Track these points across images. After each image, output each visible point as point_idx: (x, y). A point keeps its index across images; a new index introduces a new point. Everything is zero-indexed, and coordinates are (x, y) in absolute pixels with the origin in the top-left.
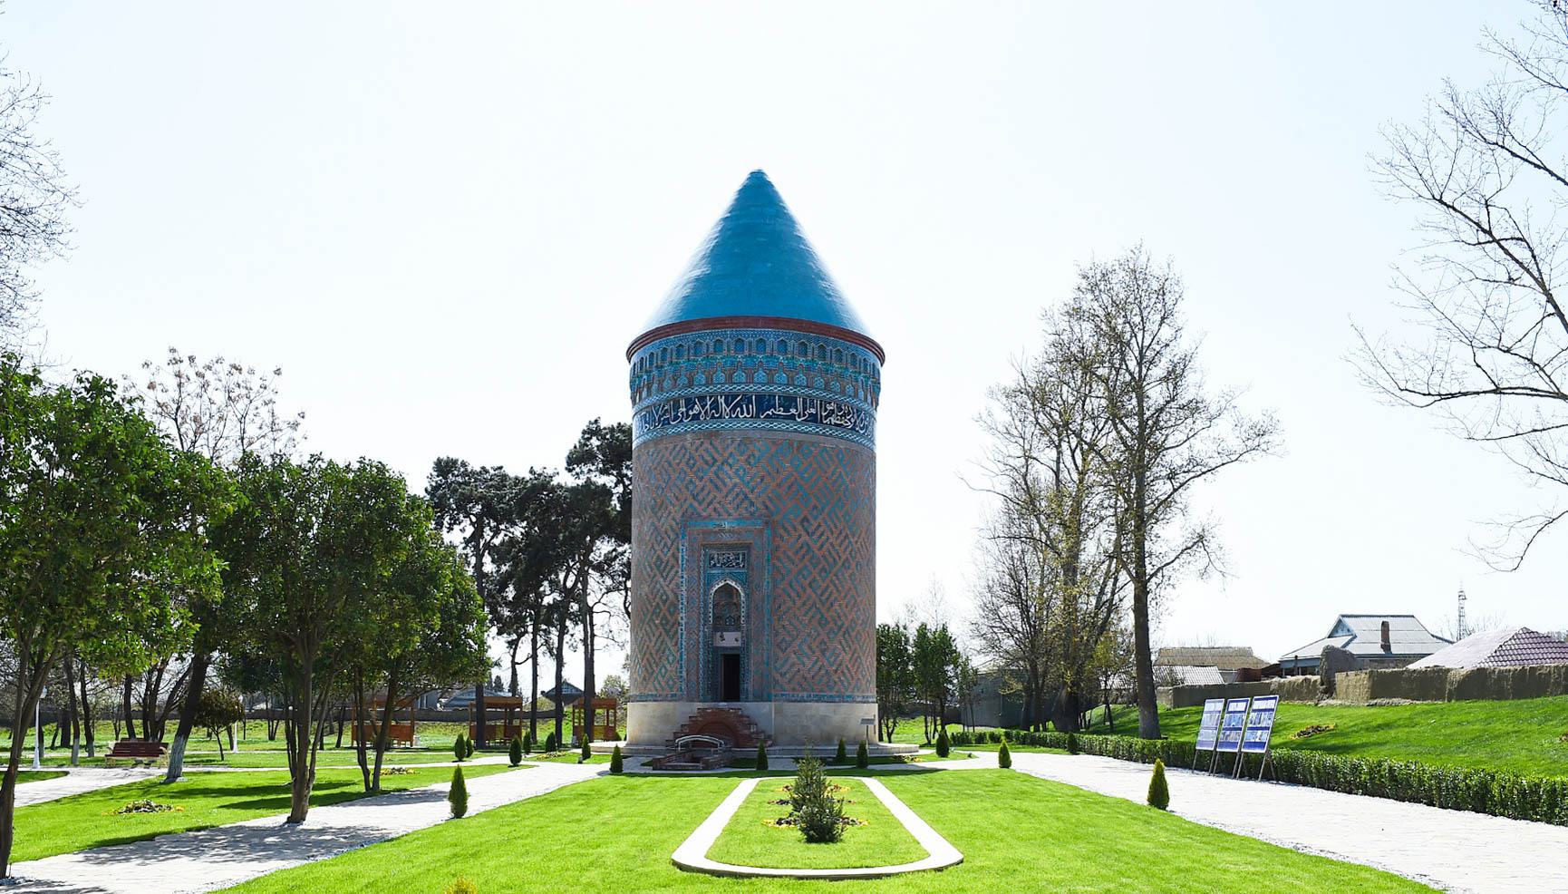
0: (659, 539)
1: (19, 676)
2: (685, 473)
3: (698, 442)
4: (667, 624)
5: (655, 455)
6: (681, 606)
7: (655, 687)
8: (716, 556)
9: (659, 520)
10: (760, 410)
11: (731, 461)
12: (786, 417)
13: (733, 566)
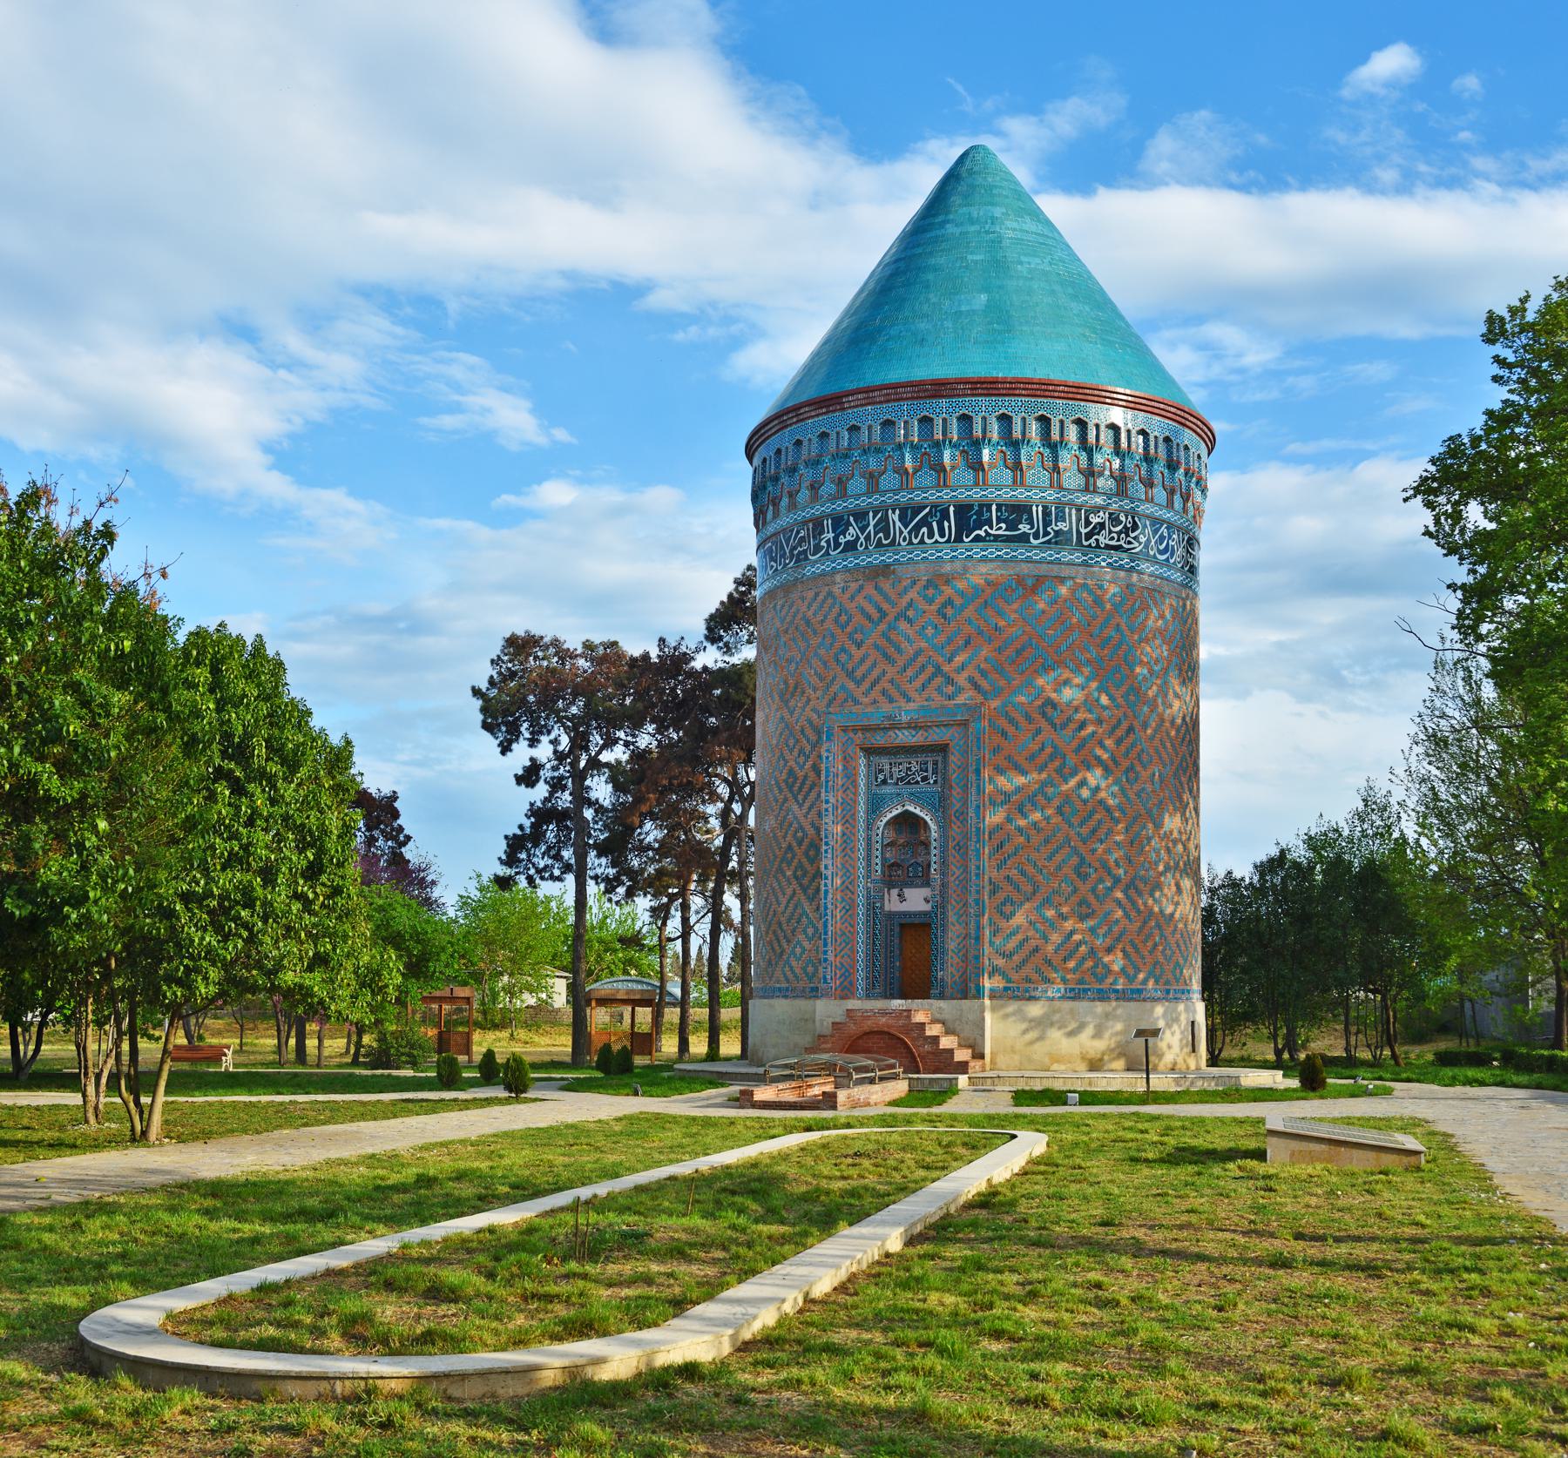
0: (791, 742)
1: (1460, 615)
2: (833, 635)
3: (854, 586)
4: (804, 875)
5: (786, 608)
6: (824, 848)
7: (785, 975)
8: (887, 767)
9: (792, 713)
10: (964, 527)
11: (910, 613)
12: (1008, 539)
13: (917, 782)
